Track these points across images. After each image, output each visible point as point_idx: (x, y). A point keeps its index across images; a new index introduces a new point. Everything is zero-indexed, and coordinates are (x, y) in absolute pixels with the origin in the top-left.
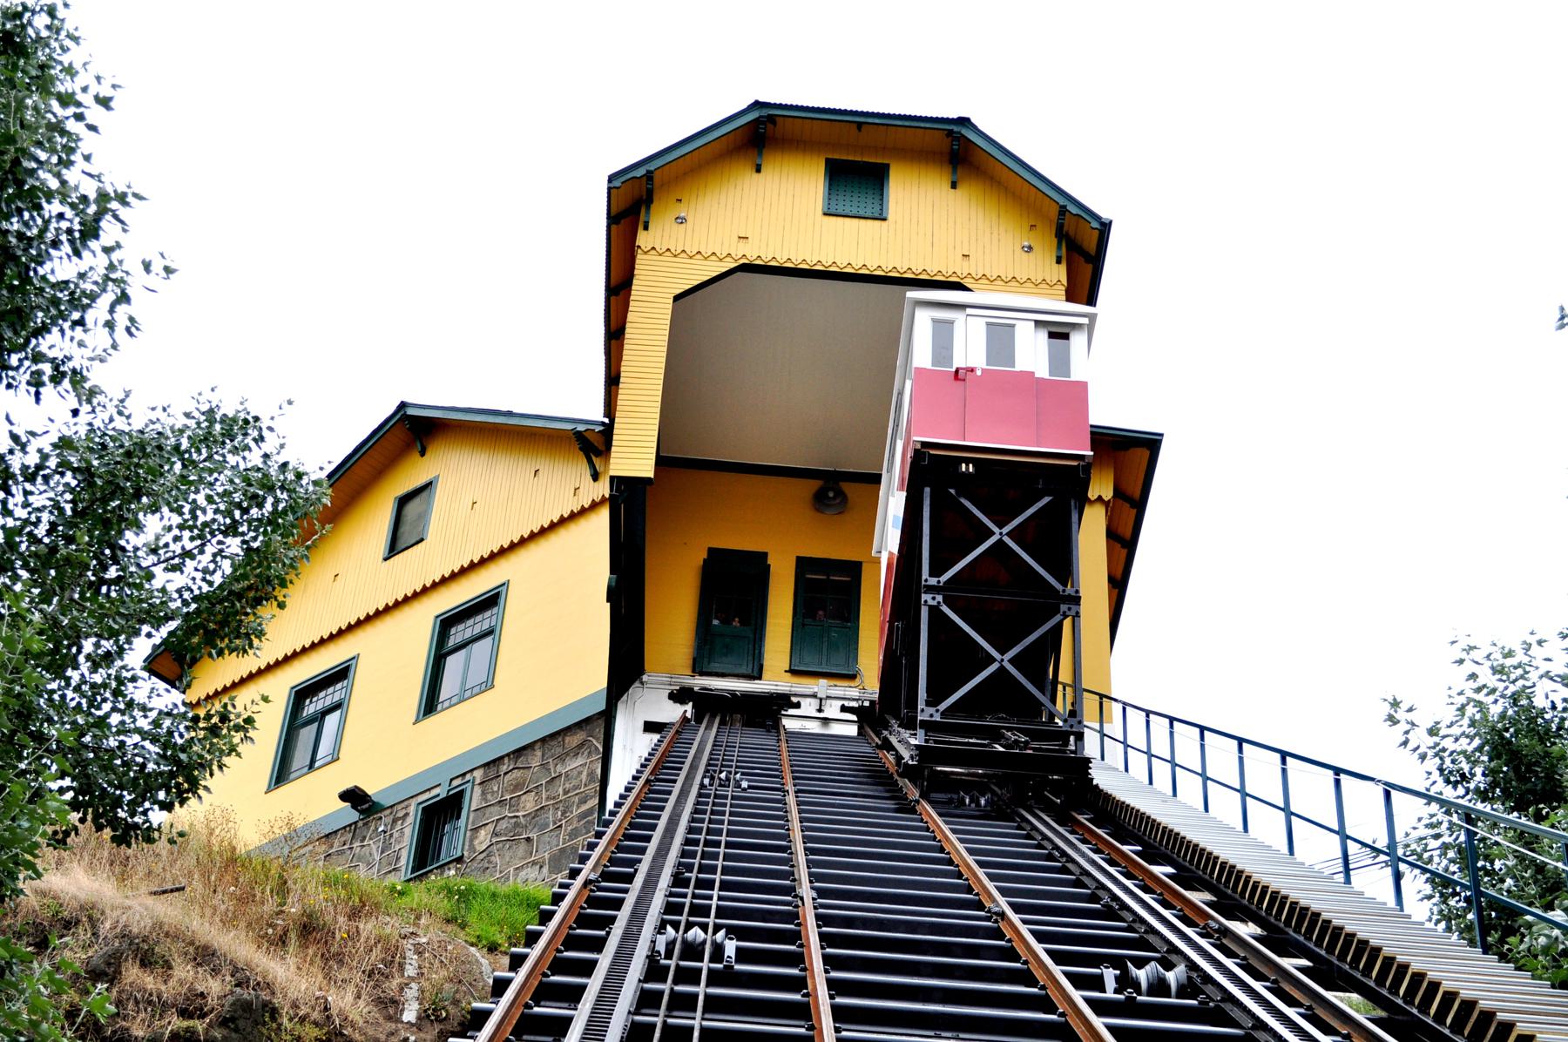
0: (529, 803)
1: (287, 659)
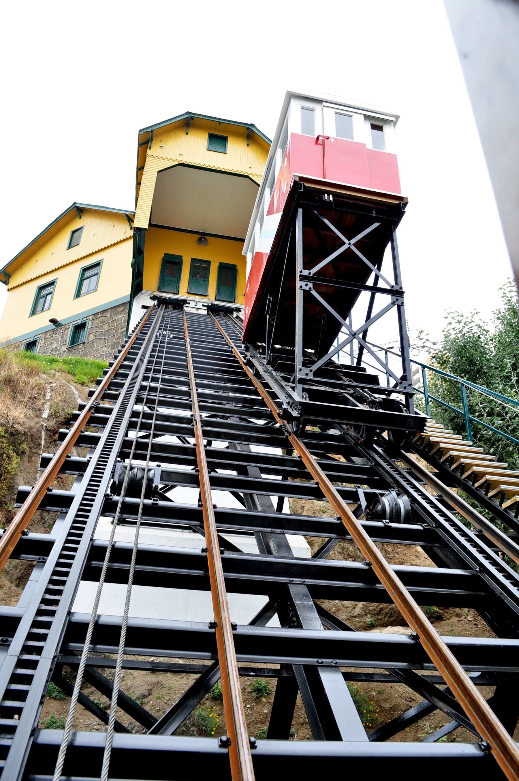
0: (106, 327)
1: (37, 278)
